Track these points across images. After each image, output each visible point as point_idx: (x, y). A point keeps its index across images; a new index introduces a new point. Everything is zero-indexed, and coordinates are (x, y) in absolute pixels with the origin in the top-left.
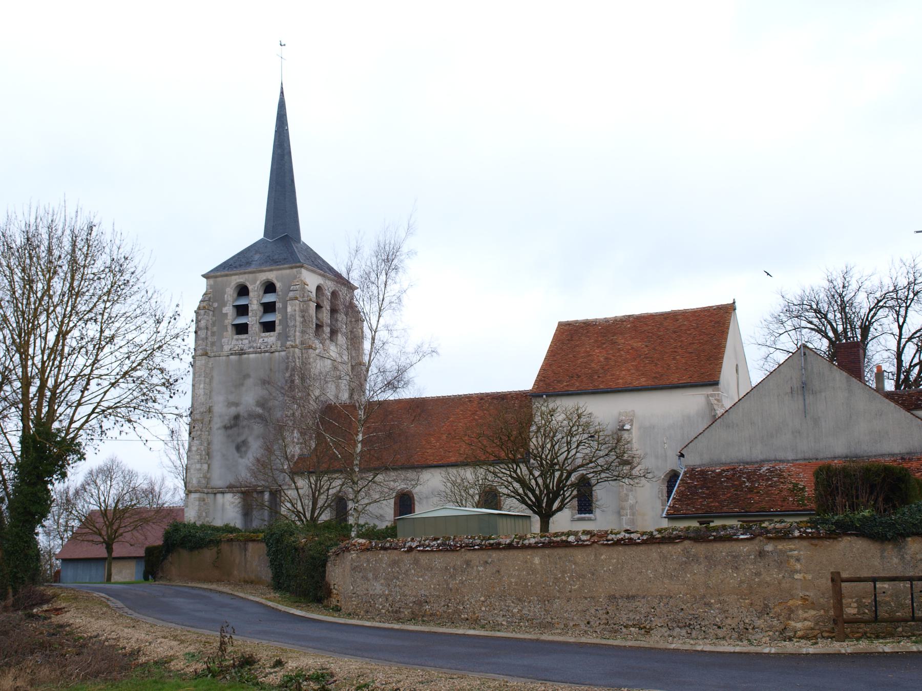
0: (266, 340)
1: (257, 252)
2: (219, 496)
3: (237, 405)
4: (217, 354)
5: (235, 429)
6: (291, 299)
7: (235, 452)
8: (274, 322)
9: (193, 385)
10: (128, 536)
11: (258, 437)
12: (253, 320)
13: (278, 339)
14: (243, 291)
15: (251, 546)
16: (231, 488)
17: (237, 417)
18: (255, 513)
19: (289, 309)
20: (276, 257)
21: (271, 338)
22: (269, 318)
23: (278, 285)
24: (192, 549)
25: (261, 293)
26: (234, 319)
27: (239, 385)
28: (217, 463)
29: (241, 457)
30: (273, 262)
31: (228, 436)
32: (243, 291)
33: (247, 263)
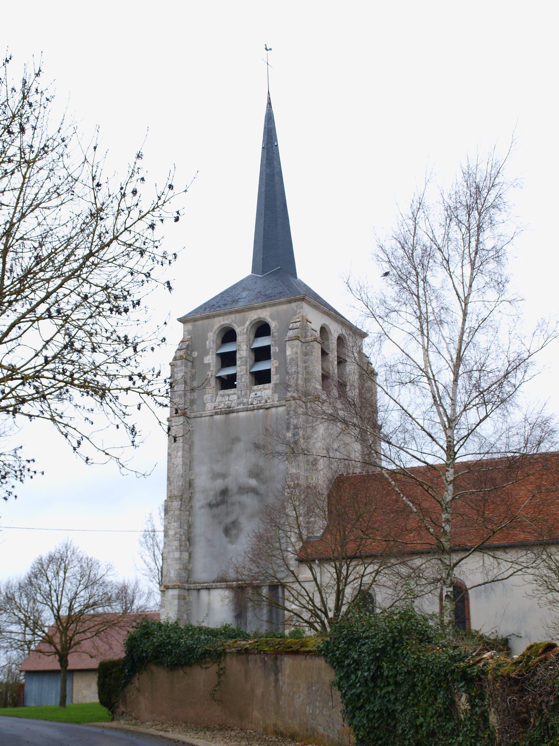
0: (259, 393)
1: (244, 289)
2: (204, 593)
3: (223, 476)
4: (198, 414)
5: (223, 507)
6: (291, 340)
7: (222, 535)
8: (270, 370)
9: (169, 455)
10: (86, 645)
11: (252, 516)
12: (241, 370)
13: (275, 392)
14: (229, 335)
15: (287, 662)
16: (222, 581)
17: (224, 492)
18: (250, 615)
19: (289, 352)
20: (269, 292)
21: (265, 392)
22: (262, 366)
23: (273, 325)
24: (174, 666)
25: (252, 336)
26: (219, 371)
27: (226, 451)
28: (200, 550)
29: (232, 542)
30: (268, 299)
31: (214, 516)
32: (229, 335)
33: (233, 301)
